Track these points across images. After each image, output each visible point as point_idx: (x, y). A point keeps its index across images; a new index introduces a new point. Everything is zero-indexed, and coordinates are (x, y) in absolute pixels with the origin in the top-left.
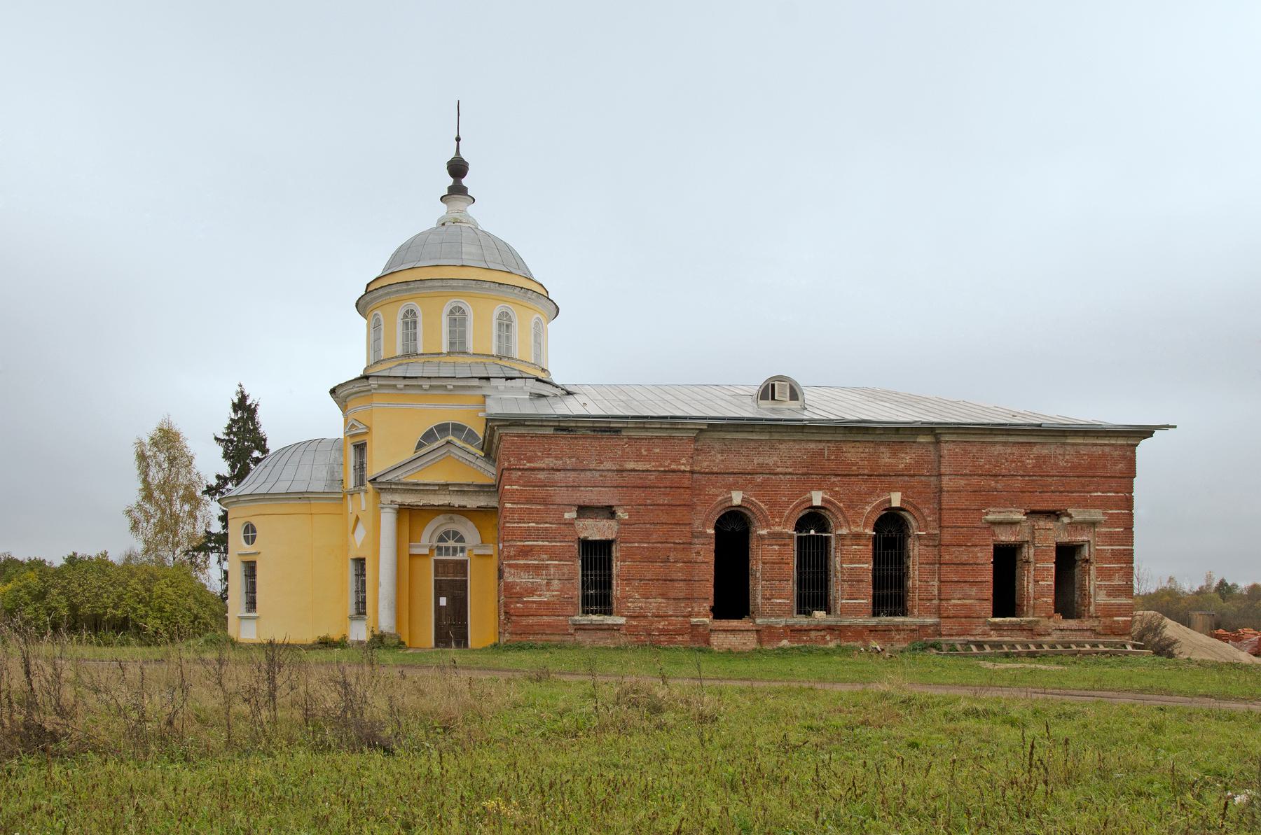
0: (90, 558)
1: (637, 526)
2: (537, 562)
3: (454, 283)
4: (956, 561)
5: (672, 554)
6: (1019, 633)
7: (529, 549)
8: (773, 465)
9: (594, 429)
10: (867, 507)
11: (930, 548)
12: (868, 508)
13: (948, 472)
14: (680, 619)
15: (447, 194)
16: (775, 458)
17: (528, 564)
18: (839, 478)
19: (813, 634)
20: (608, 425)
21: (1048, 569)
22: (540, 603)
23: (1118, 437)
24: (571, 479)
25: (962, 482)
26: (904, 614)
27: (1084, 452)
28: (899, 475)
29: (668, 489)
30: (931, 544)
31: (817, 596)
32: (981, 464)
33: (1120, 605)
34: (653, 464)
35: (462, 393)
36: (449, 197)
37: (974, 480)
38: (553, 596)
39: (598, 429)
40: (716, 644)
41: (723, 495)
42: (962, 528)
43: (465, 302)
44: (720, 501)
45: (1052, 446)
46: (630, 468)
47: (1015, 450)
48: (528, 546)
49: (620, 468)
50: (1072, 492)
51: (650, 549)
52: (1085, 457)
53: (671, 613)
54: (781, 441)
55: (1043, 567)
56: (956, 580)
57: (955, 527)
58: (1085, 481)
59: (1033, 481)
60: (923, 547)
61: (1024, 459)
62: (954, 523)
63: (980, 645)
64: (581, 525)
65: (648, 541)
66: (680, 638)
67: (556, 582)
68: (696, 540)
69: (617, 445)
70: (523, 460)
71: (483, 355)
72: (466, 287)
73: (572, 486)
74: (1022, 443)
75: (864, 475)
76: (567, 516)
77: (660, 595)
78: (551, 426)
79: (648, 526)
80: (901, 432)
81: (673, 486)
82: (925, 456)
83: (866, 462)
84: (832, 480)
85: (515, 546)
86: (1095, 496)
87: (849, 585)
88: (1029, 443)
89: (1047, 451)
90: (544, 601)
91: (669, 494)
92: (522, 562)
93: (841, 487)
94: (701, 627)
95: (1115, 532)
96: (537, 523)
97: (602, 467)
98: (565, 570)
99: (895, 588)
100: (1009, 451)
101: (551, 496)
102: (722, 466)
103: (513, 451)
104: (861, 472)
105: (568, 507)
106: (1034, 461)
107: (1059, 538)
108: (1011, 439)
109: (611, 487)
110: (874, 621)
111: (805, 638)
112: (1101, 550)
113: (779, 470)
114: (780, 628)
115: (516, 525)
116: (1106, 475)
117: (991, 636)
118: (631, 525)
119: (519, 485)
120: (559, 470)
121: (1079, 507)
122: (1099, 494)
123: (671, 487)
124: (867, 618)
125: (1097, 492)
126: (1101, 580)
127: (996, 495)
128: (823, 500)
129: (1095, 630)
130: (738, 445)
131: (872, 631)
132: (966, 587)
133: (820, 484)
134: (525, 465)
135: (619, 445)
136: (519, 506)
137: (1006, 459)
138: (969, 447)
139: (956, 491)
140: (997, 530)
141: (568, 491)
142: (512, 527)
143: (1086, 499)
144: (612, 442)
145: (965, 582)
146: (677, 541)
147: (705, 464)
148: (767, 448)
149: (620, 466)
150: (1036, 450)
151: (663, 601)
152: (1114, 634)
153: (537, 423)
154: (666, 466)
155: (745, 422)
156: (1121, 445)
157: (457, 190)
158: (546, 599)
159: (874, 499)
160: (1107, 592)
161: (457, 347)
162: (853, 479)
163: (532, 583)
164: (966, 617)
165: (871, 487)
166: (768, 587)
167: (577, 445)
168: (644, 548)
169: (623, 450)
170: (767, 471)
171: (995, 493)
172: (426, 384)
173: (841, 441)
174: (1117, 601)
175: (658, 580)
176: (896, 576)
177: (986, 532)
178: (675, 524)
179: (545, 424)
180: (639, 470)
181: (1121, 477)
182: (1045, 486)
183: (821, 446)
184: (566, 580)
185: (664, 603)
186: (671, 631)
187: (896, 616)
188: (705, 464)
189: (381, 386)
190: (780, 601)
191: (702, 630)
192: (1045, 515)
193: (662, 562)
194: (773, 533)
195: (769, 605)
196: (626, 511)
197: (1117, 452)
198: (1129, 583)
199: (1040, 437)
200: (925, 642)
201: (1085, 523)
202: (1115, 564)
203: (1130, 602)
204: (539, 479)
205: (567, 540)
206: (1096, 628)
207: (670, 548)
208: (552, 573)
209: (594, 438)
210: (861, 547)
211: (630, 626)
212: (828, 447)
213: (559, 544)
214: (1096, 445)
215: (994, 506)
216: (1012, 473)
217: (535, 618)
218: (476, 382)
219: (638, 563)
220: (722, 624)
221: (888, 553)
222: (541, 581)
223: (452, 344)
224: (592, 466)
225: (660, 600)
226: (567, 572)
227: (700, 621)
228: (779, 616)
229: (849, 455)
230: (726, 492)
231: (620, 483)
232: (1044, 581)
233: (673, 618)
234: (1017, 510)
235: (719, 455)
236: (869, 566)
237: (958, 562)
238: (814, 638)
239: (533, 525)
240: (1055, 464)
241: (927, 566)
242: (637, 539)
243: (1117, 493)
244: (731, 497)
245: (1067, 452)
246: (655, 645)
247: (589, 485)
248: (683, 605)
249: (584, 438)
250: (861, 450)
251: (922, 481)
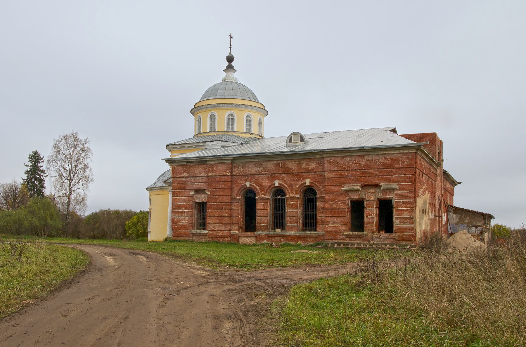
1: (213, 196)
2: (181, 211)
4: (330, 207)
6: (359, 239)
9: (198, 162)
12: (297, 186)
14: (226, 231)
16: (262, 168)
17: (179, 211)
18: (286, 175)
19: (276, 238)
20: (201, 160)
21: (372, 211)
22: (182, 225)
23: (400, 150)
24: (192, 180)
25: (333, 174)
26: (316, 231)
27: (388, 157)
30: (323, 201)
32: (341, 165)
33: (407, 227)
34: (218, 173)
35: (199, 148)
36: (226, 70)
37: (339, 173)
38: (186, 223)
40: (241, 241)
42: (334, 193)
43: (216, 113)
45: (373, 156)
48: (179, 205)
50: (384, 176)
52: (389, 160)
53: (223, 229)
54: (263, 162)
55: (370, 210)
57: (330, 193)
58: (390, 170)
59: (365, 171)
61: (360, 162)
62: (330, 191)
63: (339, 244)
65: (216, 202)
66: (226, 239)
67: (187, 218)
75: (295, 173)
76: (191, 193)
77: (220, 222)
79: (217, 196)
80: (306, 154)
83: (296, 168)
84: (283, 176)
86: (394, 177)
90: (183, 225)
94: (235, 235)
95: (404, 193)
96: (182, 196)
97: (201, 175)
102: (243, 172)
104: (294, 172)
107: (378, 197)
108: (354, 154)
109: (205, 182)
110: (303, 233)
111: (273, 240)
112: (397, 201)
114: (263, 236)
115: (175, 197)
116: (399, 167)
117: (347, 240)
118: (211, 196)
119: (177, 183)
120: (189, 177)
122: (397, 176)
124: (297, 232)
126: (397, 216)
127: (348, 179)
128: (279, 184)
129: (394, 238)
134: (178, 176)
137: (352, 163)
138: (336, 159)
139: (331, 178)
140: (350, 194)
143: (390, 179)
144: (205, 166)
145: (335, 217)
147: (237, 172)
148: (259, 165)
150: (366, 158)
151: (221, 225)
152: (403, 240)
154: (222, 174)
157: (230, 67)
160: (400, 221)
161: (212, 130)
162: (292, 175)
163: (180, 218)
164: (335, 232)
167: (194, 168)
168: (215, 204)
174: (405, 225)
175: (219, 217)
177: (344, 195)
178: (225, 195)
179: (182, 161)
180: (213, 176)
181: (407, 168)
182: (370, 173)
183: (278, 162)
187: (312, 231)
188: (237, 172)
190: (264, 225)
192: (371, 186)
194: (260, 198)
196: (208, 191)
197: (405, 156)
198: (411, 217)
200: (318, 244)
201: (391, 189)
202: (404, 208)
203: (411, 225)
204: (183, 181)
207: (223, 204)
209: (199, 165)
210: (294, 203)
211: (210, 234)
212: (281, 162)
215: (348, 183)
217: (181, 231)
218: (201, 144)
220: (248, 234)
222: (182, 217)
223: (211, 128)
224: (198, 175)
225: (220, 224)
232: (370, 216)
235: (242, 168)
239: (181, 197)
240: (375, 164)
241: (322, 210)
242: (212, 201)
243: (406, 175)
248: (227, 226)
251: (319, 174)
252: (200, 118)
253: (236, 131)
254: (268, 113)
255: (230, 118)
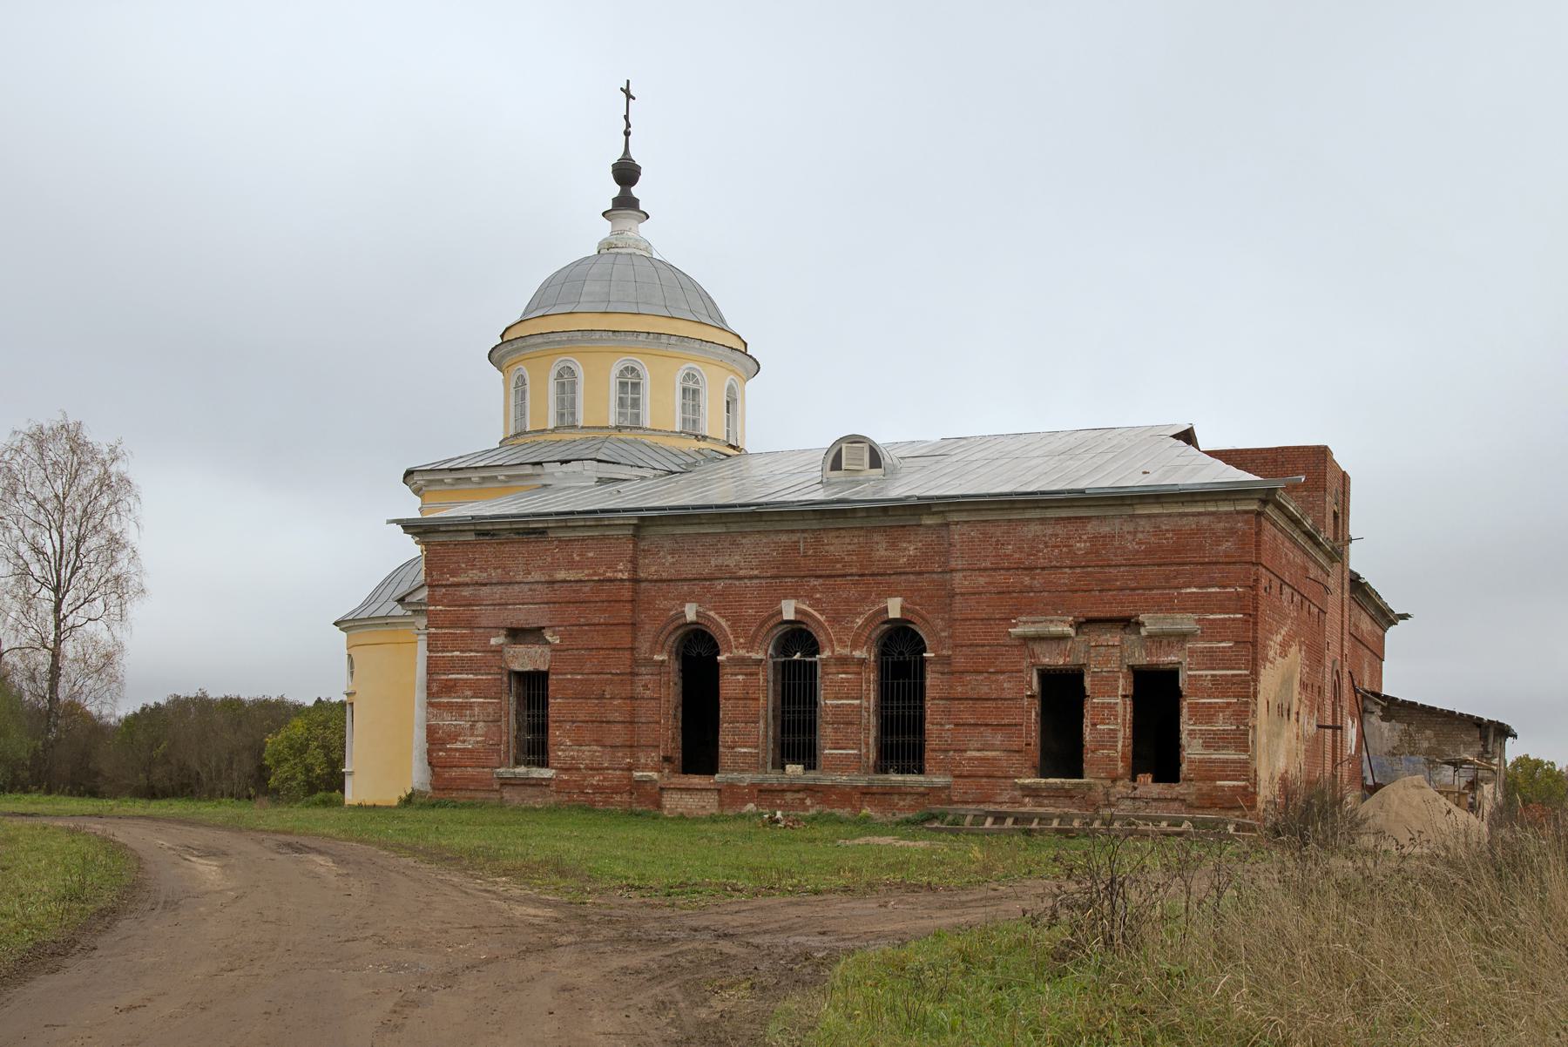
0: (157, 704)
1: (570, 652)
2: (461, 700)
3: (556, 337)
4: (971, 694)
5: (608, 688)
7: (452, 683)
8: (735, 566)
9: (517, 532)
10: (857, 620)
11: (946, 676)
12: (860, 621)
13: (960, 567)
14: (618, 772)
15: (611, 208)
22: (464, 750)
24: (498, 596)
25: (982, 581)
27: (1168, 527)
28: (900, 574)
29: (606, 604)
31: (804, 743)
32: (1008, 552)
33: (1226, 761)
34: (586, 572)
37: (1000, 577)
38: (478, 742)
39: (521, 531)
40: (668, 806)
41: (676, 609)
43: (578, 364)
44: (709, 616)
46: (560, 579)
47: (1059, 530)
48: (451, 680)
49: (550, 579)
51: (584, 682)
54: (744, 534)
55: (1103, 703)
56: (972, 721)
57: (971, 645)
58: (1170, 571)
59: (1088, 574)
60: (937, 675)
61: (1071, 542)
63: (999, 818)
64: (512, 652)
66: (618, 798)
67: (481, 724)
68: (643, 669)
69: (547, 550)
70: (445, 573)
71: (594, 428)
72: (571, 340)
73: (499, 605)
74: (1069, 518)
75: (851, 575)
77: (594, 740)
78: (630, 524)
81: (611, 599)
82: (935, 545)
83: (854, 557)
84: (812, 584)
85: (438, 680)
86: (1186, 593)
87: (834, 729)
88: (1081, 518)
89: (1108, 529)
91: (606, 610)
92: (446, 701)
93: (824, 593)
95: (1219, 648)
96: (462, 651)
97: (530, 579)
98: (490, 710)
99: (909, 733)
100: (1049, 532)
101: (476, 617)
103: (436, 563)
105: (494, 630)
106: (1088, 544)
107: (1133, 659)
108: (1051, 513)
111: (778, 802)
112: (1195, 676)
113: (742, 573)
114: (744, 787)
115: (440, 654)
117: (1025, 805)
118: (564, 651)
120: (485, 585)
121: (1161, 611)
122: (1194, 590)
123: (610, 602)
124: (857, 776)
125: (1189, 587)
126: (1195, 724)
127: (1032, 597)
128: (797, 611)
129: (1184, 800)
130: (692, 542)
131: (866, 794)
132: (988, 732)
133: (796, 590)
135: (549, 549)
136: (443, 631)
138: (991, 529)
139: (974, 594)
140: (1038, 648)
141: (494, 610)
142: (436, 657)
143: (1171, 599)
145: (987, 725)
146: (613, 671)
147: (653, 569)
148: (726, 544)
149: (549, 576)
150: (1091, 528)
151: (599, 749)
153: (451, 528)
155: (691, 512)
156: (1227, 513)
157: (625, 203)
158: (470, 746)
159: (867, 608)
160: (1204, 742)
161: (566, 421)
162: (839, 581)
163: (455, 726)
164: (989, 777)
165: (863, 591)
166: (730, 731)
168: (578, 680)
169: (553, 556)
170: (727, 575)
171: (1032, 594)
172: (475, 476)
173: (819, 530)
175: (592, 722)
176: (909, 716)
180: (570, 581)
182: (1107, 581)
183: (795, 537)
184: (491, 722)
185: (599, 752)
186: (607, 788)
187: (909, 773)
188: (653, 569)
189: (431, 482)
191: (649, 788)
193: (597, 699)
195: (731, 756)
197: (1222, 525)
199: (1092, 509)
202: (1218, 698)
203: (1242, 757)
205: (492, 672)
206: (1186, 796)
207: (607, 680)
208: (476, 713)
210: (849, 676)
212: (804, 538)
213: (484, 677)
214: (1186, 515)
215: (1030, 614)
216: (1054, 563)
217: (459, 770)
218: (529, 470)
219: (570, 700)
221: (898, 684)
223: (561, 416)
224: (519, 578)
226: (492, 712)
227: (646, 776)
228: (743, 770)
229: (832, 548)
230: (679, 605)
231: (551, 597)
233: (610, 772)
234: (1062, 618)
235: (669, 557)
236: (871, 701)
237: (975, 696)
238: (790, 802)
239: (457, 653)
244: (683, 612)
245: (1140, 529)
246: (589, 808)
247: (518, 602)
248: (620, 754)
249: (511, 542)
250: (847, 540)
251: (934, 581)
252: (521, 379)
253: (648, 427)
254: (758, 365)
255: (627, 383)
